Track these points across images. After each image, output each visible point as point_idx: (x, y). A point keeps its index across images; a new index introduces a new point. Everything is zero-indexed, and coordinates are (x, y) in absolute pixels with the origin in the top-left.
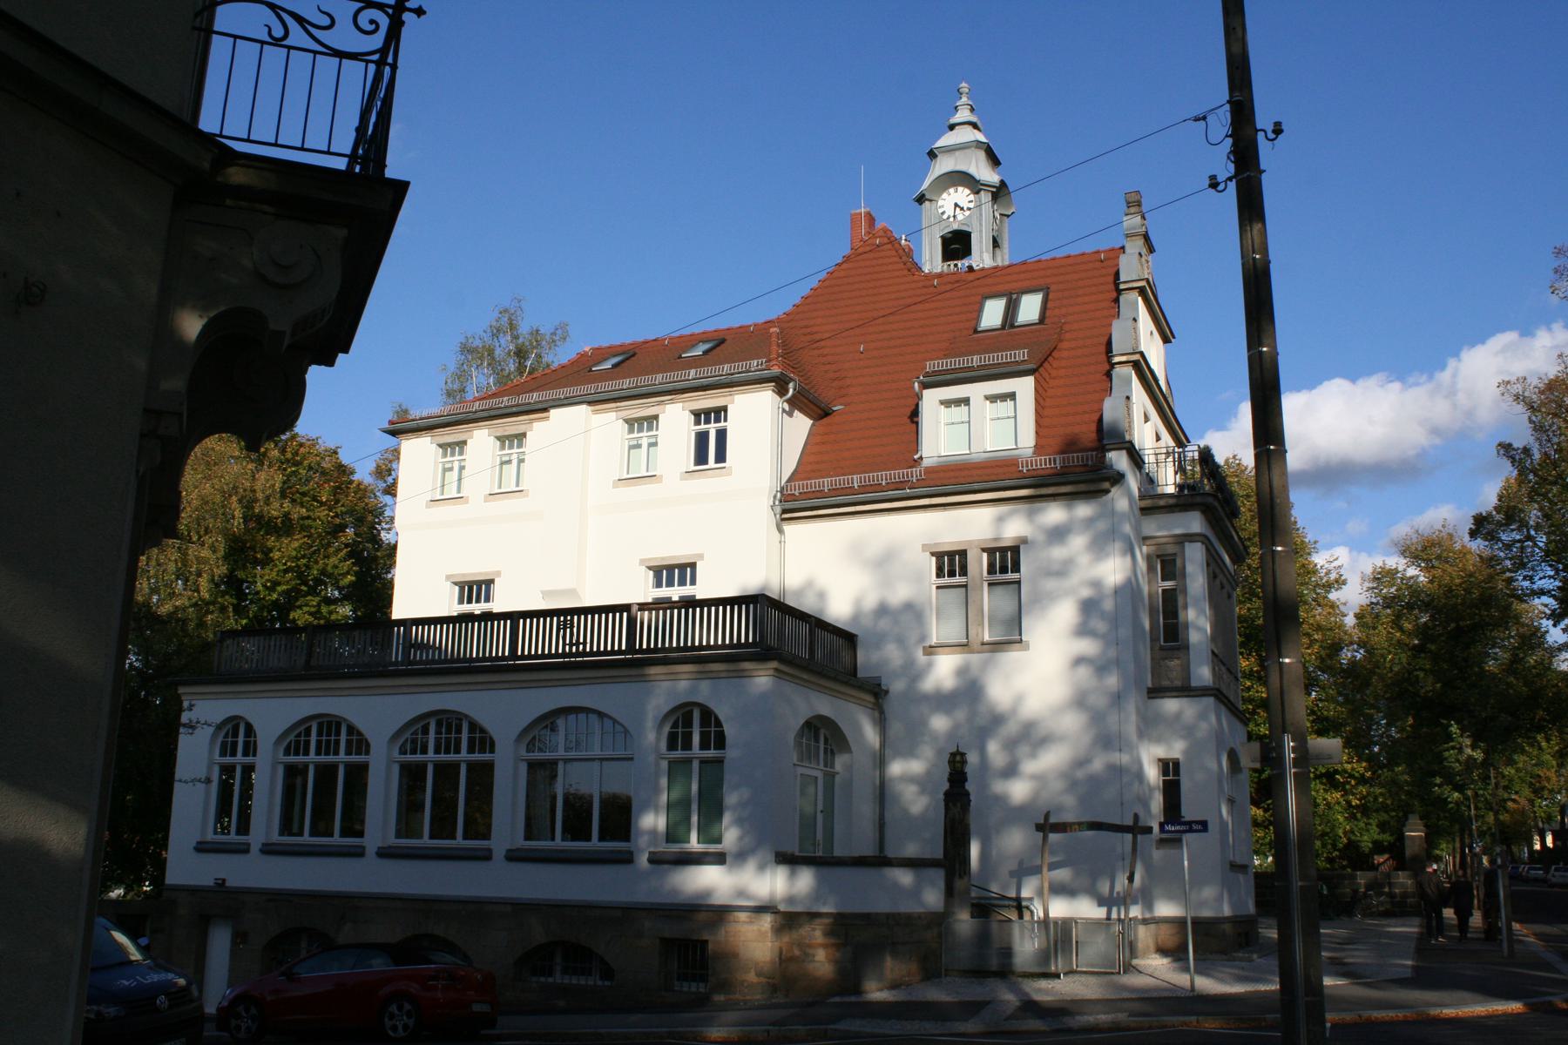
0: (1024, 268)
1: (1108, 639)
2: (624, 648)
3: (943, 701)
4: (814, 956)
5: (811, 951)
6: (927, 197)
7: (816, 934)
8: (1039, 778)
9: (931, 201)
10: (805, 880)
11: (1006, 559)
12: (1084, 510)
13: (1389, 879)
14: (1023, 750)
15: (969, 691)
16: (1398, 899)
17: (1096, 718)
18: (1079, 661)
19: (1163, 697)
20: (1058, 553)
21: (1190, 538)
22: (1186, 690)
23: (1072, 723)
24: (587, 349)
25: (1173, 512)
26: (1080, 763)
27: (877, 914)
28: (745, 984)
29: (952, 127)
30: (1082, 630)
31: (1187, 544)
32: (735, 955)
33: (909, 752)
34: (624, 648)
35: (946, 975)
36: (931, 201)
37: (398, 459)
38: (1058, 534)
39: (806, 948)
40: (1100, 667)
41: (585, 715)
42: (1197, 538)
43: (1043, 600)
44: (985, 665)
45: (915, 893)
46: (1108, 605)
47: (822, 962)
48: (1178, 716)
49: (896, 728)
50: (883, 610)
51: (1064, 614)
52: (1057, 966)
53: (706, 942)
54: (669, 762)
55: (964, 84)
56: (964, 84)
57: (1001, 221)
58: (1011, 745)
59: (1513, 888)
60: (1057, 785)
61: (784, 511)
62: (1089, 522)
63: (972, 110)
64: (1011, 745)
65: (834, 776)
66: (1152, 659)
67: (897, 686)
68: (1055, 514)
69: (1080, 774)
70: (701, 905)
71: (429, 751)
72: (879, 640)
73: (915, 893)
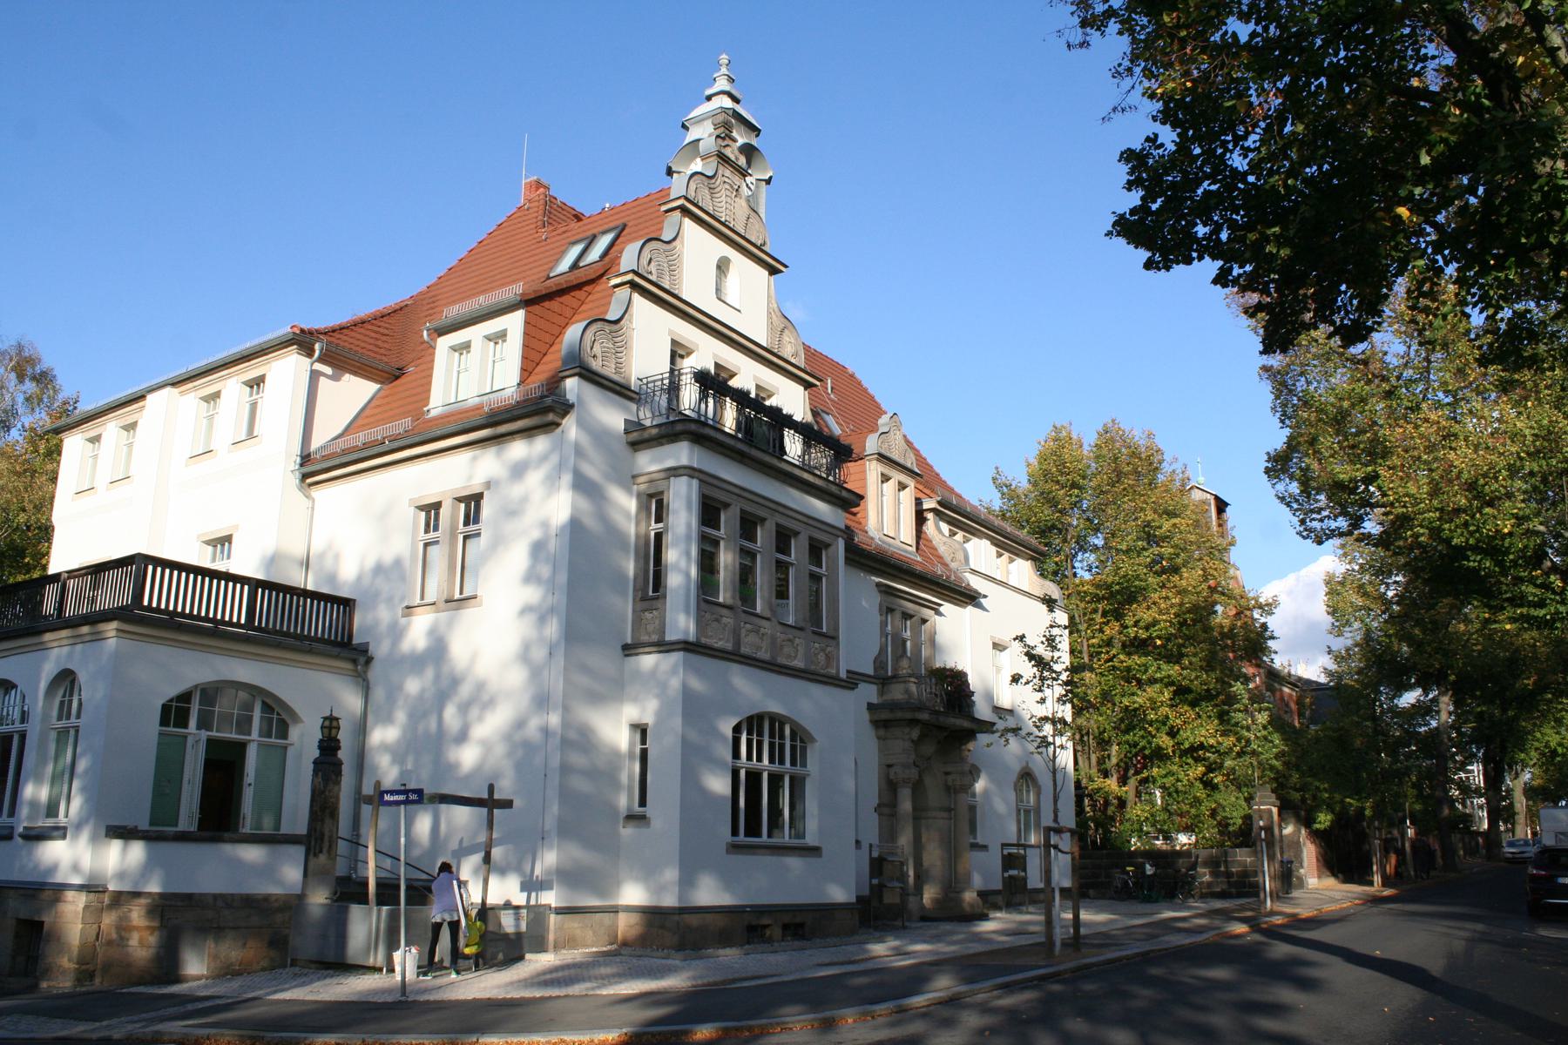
0: (625, 207)
1: (551, 585)
2: (243, 621)
3: (417, 662)
4: (128, 940)
5: (127, 935)
6: (674, 169)
7: (137, 915)
8: (486, 745)
9: (679, 172)
10: (137, 851)
11: (472, 503)
12: (541, 443)
13: (1226, 857)
14: (474, 712)
15: (438, 650)
16: (1235, 879)
17: (535, 673)
18: (526, 610)
19: (637, 654)
20: (517, 491)
21: (673, 472)
22: (663, 646)
23: (516, 677)
24: (1199, 479)
25: (662, 444)
26: (520, 724)
27: (201, 895)
28: (61, 970)
29: (709, 98)
30: (530, 577)
31: (672, 479)
32: (59, 939)
33: (388, 719)
34: (243, 621)
35: (292, 965)
36: (679, 172)
37: (1331, 593)
38: (519, 470)
39: (123, 928)
40: (541, 615)
41: (234, 691)
42: (681, 471)
43: (498, 542)
44: (450, 624)
45: (268, 871)
46: (552, 545)
47: (141, 944)
48: (653, 672)
49: (378, 693)
50: (379, 569)
51: (516, 558)
52: (375, 958)
53: (43, 922)
54: (59, 732)
55: (724, 56)
56: (724, 56)
57: (757, 187)
58: (464, 708)
59: (1006, 875)
60: (500, 750)
61: (305, 476)
62: (544, 458)
63: (731, 80)
64: (464, 708)
65: (186, 737)
66: (634, 611)
67: (380, 650)
68: (518, 449)
69: (517, 737)
70: (45, 884)
71: (253, 732)
72: (374, 597)
73: (268, 871)
